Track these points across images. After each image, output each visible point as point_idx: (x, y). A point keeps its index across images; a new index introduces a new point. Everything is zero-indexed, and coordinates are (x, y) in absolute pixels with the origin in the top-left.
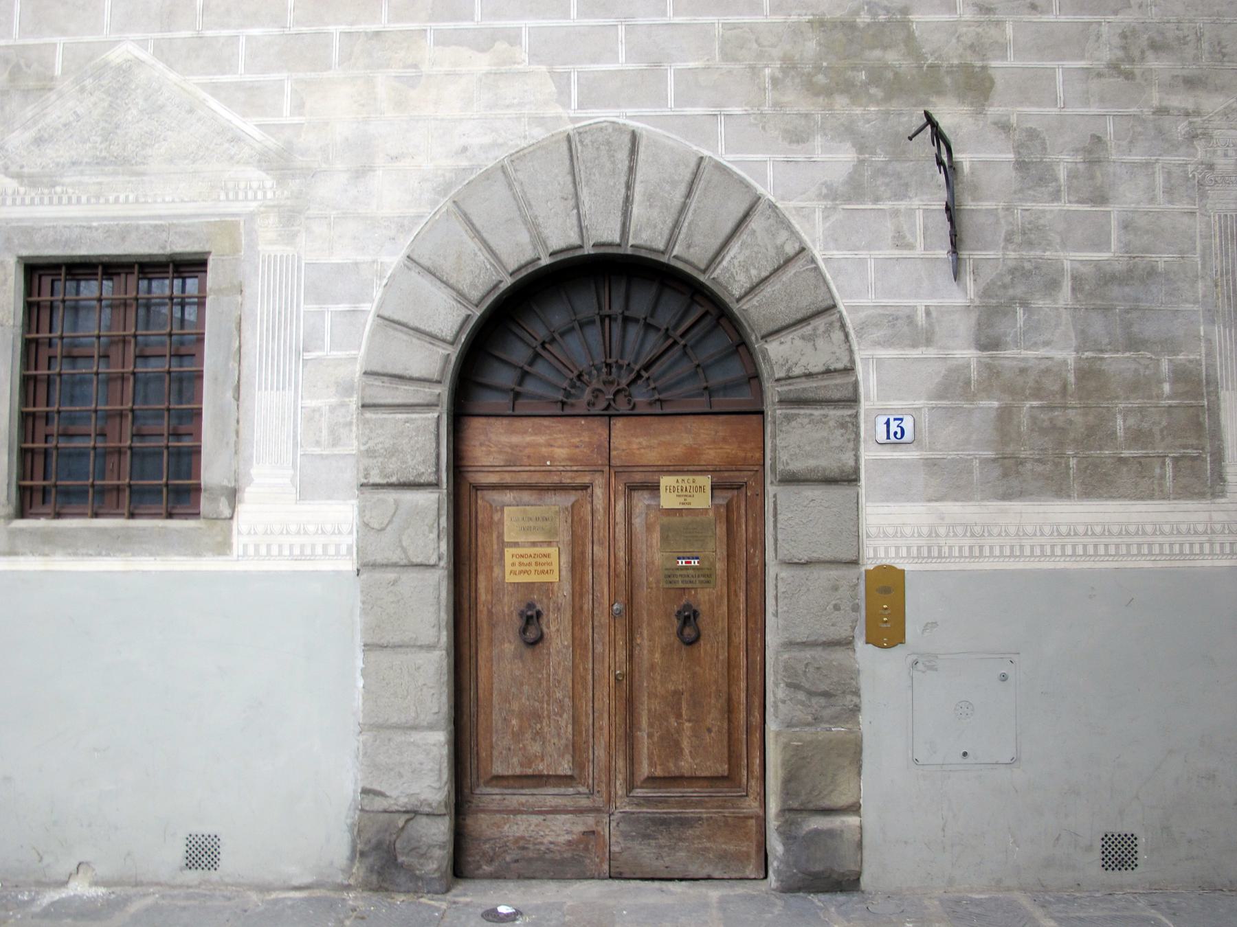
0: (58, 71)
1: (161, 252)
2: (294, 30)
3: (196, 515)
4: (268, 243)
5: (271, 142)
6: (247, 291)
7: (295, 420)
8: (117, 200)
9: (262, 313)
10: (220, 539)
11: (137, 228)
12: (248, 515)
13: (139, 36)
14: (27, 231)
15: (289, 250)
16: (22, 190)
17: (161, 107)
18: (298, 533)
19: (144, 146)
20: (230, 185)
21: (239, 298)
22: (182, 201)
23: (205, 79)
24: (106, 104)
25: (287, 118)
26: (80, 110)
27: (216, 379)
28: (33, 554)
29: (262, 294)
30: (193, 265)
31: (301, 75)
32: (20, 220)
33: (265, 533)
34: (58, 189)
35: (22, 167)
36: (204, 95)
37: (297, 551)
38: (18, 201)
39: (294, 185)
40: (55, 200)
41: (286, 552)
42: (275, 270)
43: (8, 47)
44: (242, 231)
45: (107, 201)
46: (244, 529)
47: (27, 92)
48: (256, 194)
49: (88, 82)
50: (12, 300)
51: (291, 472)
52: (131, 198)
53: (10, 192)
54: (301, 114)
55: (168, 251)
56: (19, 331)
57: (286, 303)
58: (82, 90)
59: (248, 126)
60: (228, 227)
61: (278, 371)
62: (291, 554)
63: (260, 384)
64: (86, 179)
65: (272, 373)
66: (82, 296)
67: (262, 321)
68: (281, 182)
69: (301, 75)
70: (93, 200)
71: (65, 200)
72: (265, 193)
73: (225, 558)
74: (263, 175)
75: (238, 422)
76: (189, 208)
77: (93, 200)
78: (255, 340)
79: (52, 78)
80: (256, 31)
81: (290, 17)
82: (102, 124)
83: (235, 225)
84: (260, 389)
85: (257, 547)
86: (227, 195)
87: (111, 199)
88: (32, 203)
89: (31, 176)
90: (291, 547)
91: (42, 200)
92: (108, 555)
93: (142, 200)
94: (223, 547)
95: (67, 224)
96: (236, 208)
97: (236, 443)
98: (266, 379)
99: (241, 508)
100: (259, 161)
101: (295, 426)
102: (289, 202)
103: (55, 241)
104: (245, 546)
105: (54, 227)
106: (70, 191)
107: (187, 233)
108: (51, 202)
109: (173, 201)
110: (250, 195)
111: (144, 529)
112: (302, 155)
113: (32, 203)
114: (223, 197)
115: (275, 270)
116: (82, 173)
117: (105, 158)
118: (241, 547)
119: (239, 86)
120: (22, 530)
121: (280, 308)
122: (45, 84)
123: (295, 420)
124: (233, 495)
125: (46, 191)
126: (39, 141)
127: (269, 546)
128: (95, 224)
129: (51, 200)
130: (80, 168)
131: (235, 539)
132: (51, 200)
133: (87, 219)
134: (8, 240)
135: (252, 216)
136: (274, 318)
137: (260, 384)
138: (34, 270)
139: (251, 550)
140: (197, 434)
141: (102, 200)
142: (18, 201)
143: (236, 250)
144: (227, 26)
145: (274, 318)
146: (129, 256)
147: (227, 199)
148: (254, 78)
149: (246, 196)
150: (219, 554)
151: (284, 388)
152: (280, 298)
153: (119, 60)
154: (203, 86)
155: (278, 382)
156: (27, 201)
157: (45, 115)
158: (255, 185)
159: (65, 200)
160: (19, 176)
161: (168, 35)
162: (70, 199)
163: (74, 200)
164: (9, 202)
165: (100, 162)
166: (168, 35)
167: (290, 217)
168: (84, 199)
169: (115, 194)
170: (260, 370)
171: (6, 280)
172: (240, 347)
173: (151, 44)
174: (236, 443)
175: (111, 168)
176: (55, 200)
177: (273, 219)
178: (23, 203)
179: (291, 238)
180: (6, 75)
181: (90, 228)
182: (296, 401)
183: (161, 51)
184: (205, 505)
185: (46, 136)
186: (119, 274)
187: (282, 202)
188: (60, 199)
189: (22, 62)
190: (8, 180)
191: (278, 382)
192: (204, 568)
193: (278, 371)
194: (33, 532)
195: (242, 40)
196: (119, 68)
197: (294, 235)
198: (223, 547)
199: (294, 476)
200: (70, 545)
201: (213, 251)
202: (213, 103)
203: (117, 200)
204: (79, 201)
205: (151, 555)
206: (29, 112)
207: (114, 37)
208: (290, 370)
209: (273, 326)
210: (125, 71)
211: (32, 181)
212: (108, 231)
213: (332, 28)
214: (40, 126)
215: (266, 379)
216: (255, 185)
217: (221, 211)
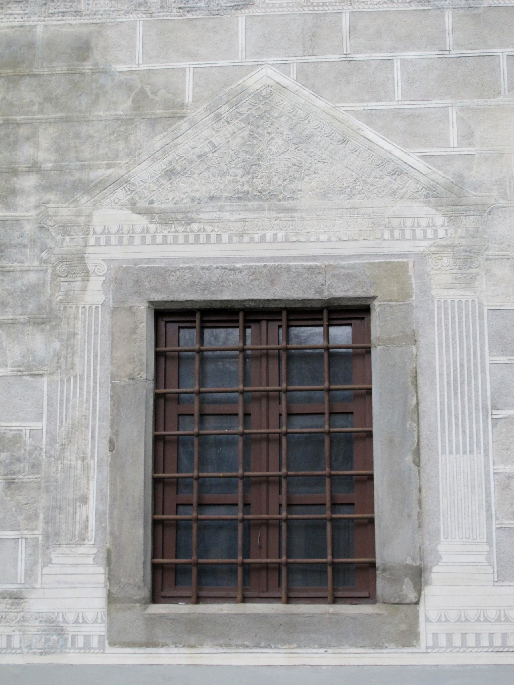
0: (189, 99)
1: (318, 297)
2: (454, 53)
3: (370, 598)
4: (440, 288)
5: (440, 176)
6: (422, 341)
7: (488, 488)
8: (263, 240)
9: (441, 366)
10: (404, 627)
11: (289, 269)
12: (438, 602)
13: (279, 60)
14: (160, 274)
15: (469, 295)
16: (153, 227)
17: (309, 137)
18: (498, 620)
19: (293, 179)
20: (395, 222)
21: (414, 349)
22: (340, 240)
23: (359, 106)
24: (246, 134)
25: (454, 145)
26: (217, 140)
27: (391, 441)
28: (176, 644)
29: (440, 344)
30: (355, 312)
31: (467, 102)
32: (150, 261)
33: (459, 620)
34: (195, 227)
35: (152, 202)
36: (358, 124)
37: (498, 642)
38: (148, 240)
39: (469, 222)
40: (192, 239)
41: (485, 643)
42: (453, 318)
43: (131, 72)
44: (411, 273)
45: (252, 240)
46: (433, 615)
47: (154, 122)
48: (425, 233)
49: (224, 110)
50: (144, 350)
51: (487, 548)
52: (280, 236)
53: (138, 229)
54: (470, 145)
55: (326, 295)
56: (151, 385)
57: (468, 354)
58: (218, 118)
59: (411, 158)
60: (395, 270)
61: (464, 432)
62: (491, 645)
63: (443, 447)
64: (226, 215)
65: (457, 434)
66: (206, 346)
67: (441, 375)
68: (453, 218)
69: (467, 102)
70: (235, 239)
71: (202, 238)
72: (436, 231)
73: (410, 650)
74: (433, 211)
75: (420, 491)
76: (348, 248)
77: (235, 239)
78: (435, 396)
79: (183, 106)
80: (411, 55)
81: (449, 40)
82: (243, 155)
83: (403, 266)
84: (444, 452)
85: (449, 636)
86: (392, 232)
87: (257, 238)
88: (165, 242)
89: (162, 212)
90: (491, 635)
91: (175, 238)
92: (268, 646)
93: (293, 239)
94: (409, 637)
95: (207, 265)
96: (403, 247)
97: (420, 514)
98: (450, 441)
99: (427, 591)
100: (427, 196)
101: (488, 495)
102: (464, 242)
103: (192, 284)
104: (435, 635)
105: (190, 268)
106: (209, 228)
107: (347, 276)
108: (186, 242)
109: (329, 240)
110: (419, 233)
111: (312, 616)
112: (475, 189)
113: (165, 242)
114: (387, 236)
115: (453, 318)
116: (221, 209)
117: (248, 193)
118: (430, 636)
119: (396, 114)
120: (162, 616)
121: (462, 360)
122: (175, 112)
123: (488, 488)
124: (418, 575)
125: (180, 228)
126: (170, 174)
127: (464, 635)
128: (239, 265)
129: (186, 237)
130: (219, 203)
131: (422, 627)
132: (186, 237)
133: (228, 259)
134: (138, 283)
135: (422, 256)
136: (455, 371)
137: (443, 447)
138: (166, 315)
139: (443, 641)
140: (368, 502)
141: (246, 239)
142: (148, 240)
143: (406, 294)
144: (379, 49)
145: (455, 371)
146: (280, 300)
147: (393, 238)
148: (415, 105)
149: (414, 235)
150: (404, 646)
151: (471, 452)
152: (461, 349)
153: (258, 86)
154: (355, 113)
155: (464, 443)
156: (159, 240)
157: (176, 145)
158: (424, 222)
159: (202, 238)
160: (148, 212)
161: (313, 59)
162: (208, 237)
163: (213, 239)
164: (138, 240)
165: (242, 197)
166: (313, 59)
167: (468, 258)
168: (225, 238)
169: (261, 232)
170: (443, 429)
171: (136, 327)
172: (418, 404)
173: (293, 68)
174: (420, 514)
175: (255, 203)
176: (192, 239)
177: (446, 261)
178: (154, 242)
179: (469, 282)
180: (130, 102)
181: (233, 269)
182: (487, 466)
183: (307, 76)
184: (382, 586)
185: (179, 168)
186: (259, 321)
187: (457, 242)
188: (197, 237)
189: (147, 89)
190: (135, 217)
191: (464, 443)
192: (387, 662)
193: (464, 432)
194: (175, 619)
195: (397, 64)
196: (258, 94)
197: (473, 279)
198: (409, 637)
199: (490, 553)
200: (223, 635)
201: (379, 296)
202: (369, 133)
203: (263, 240)
204: (219, 240)
205: (321, 646)
206: (158, 142)
207: (250, 61)
208: (478, 430)
209: (455, 380)
210: (265, 97)
211: (165, 218)
212: (254, 272)
213: (497, 51)
214: (170, 157)
215: (450, 441)
216: (424, 222)
217: (386, 251)
